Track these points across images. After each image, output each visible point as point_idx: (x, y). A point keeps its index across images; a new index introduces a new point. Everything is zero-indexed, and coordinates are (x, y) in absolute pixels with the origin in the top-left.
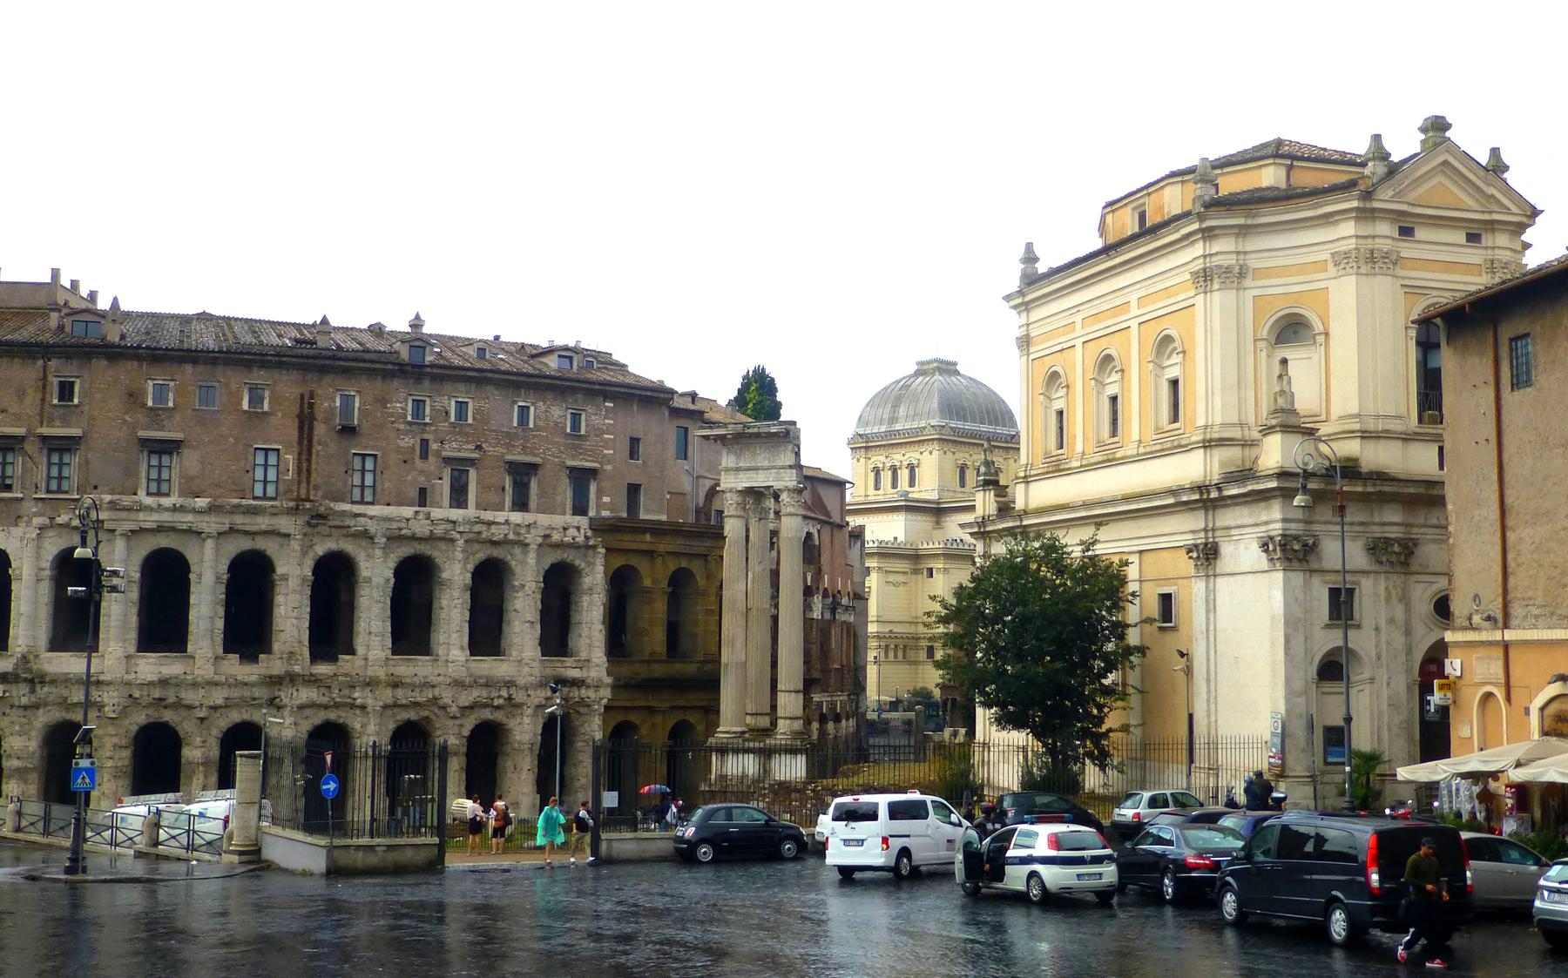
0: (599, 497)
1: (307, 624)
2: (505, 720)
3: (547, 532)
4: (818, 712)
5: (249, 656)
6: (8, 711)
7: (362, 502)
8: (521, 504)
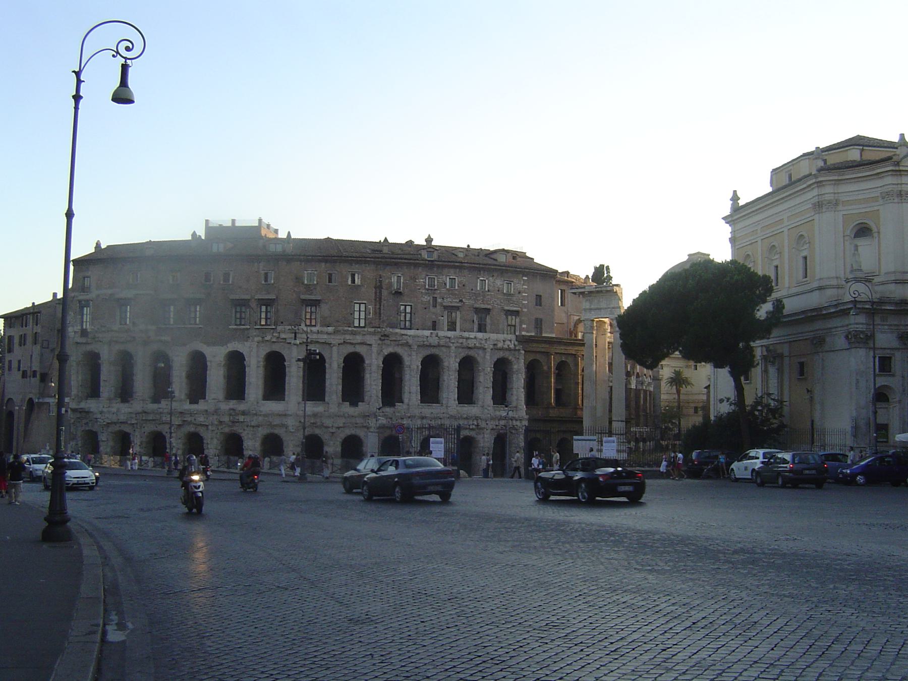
0: (521, 325)
1: (380, 388)
2: (476, 436)
3: (495, 343)
4: (634, 437)
5: (354, 404)
6: (246, 428)
7: (405, 328)
8: (482, 328)
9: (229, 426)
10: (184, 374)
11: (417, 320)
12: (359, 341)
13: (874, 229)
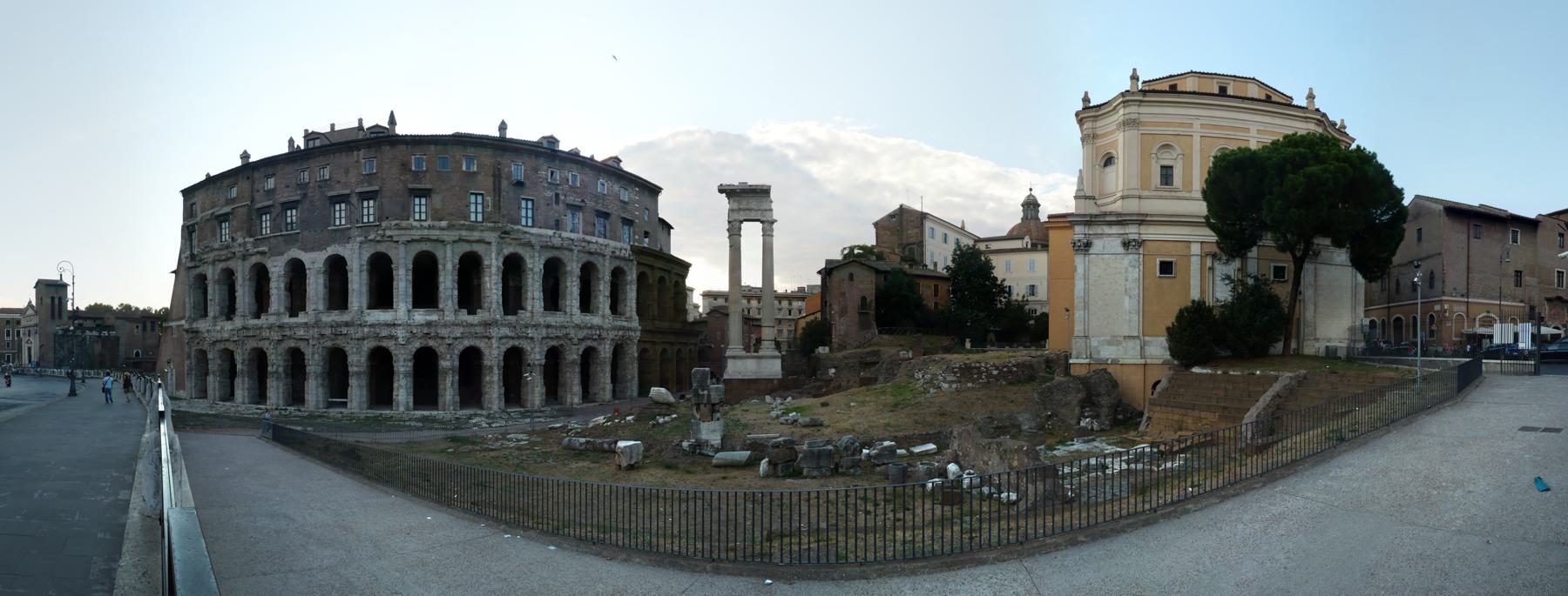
5: (471, 312)
9: (332, 340)
10: (282, 285)
11: (539, 217)
12: (477, 238)
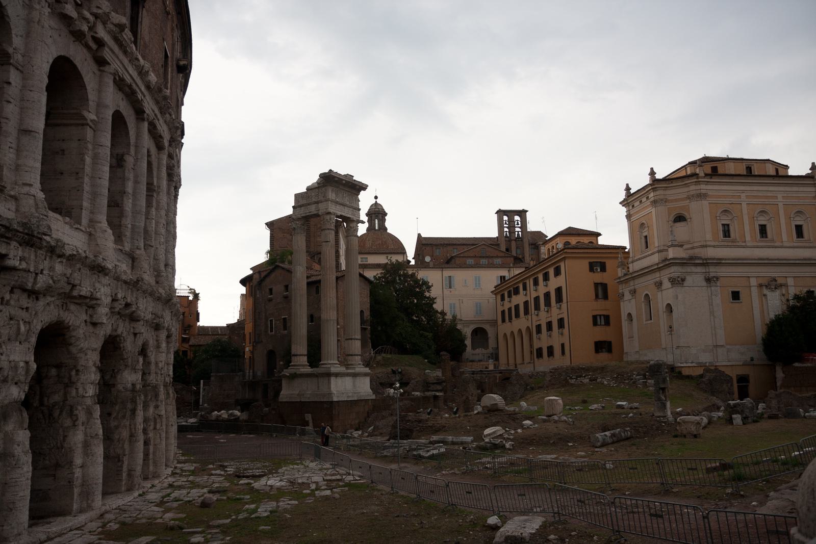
13: (687, 216)
